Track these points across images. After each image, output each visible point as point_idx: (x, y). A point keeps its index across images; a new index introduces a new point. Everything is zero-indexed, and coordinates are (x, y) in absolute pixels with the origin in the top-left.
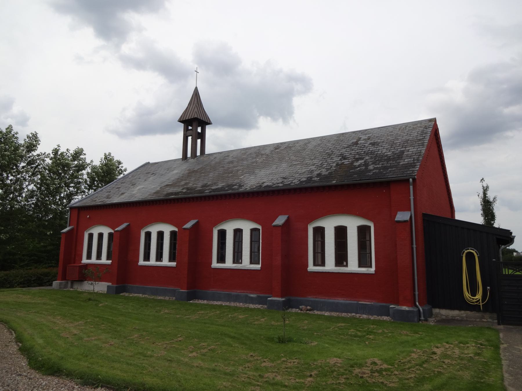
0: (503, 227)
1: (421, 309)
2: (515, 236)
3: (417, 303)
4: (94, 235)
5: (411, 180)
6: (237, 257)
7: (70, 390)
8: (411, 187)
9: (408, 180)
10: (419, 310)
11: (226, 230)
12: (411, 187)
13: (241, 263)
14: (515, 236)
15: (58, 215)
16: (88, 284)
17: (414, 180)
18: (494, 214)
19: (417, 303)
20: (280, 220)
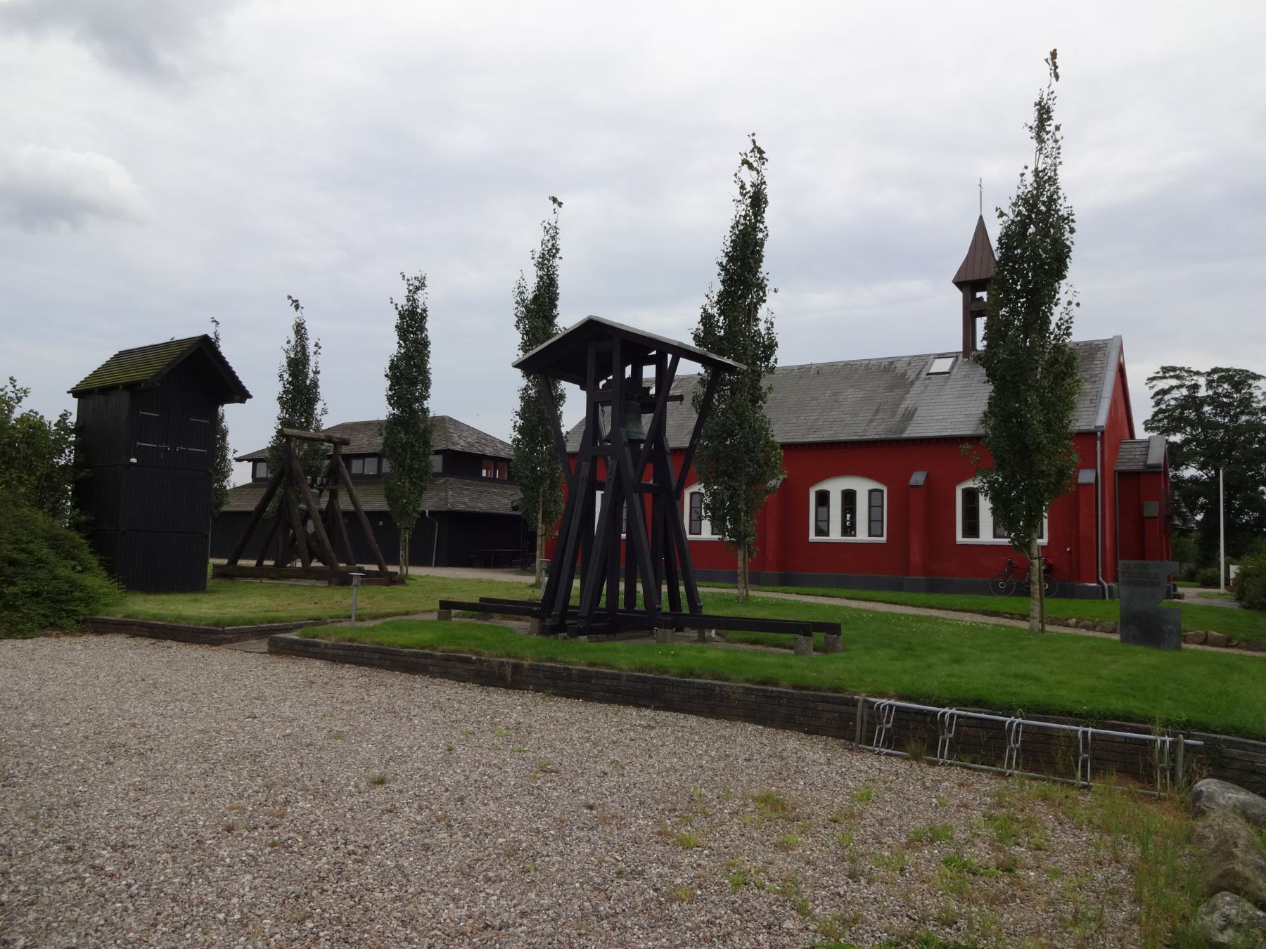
0: (438, 414)
1: (1106, 585)
2: (250, 397)
3: (1101, 579)
4: (226, 350)
5: (1099, 433)
6: (849, 529)
7: (725, 938)
8: (1099, 442)
9: (1096, 433)
10: (1103, 587)
11: (855, 491)
12: (1099, 442)
13: (855, 535)
14: (250, 397)
15: (1035, 264)
16: (327, 405)
17: (1102, 433)
18: (520, 422)
19: (1101, 579)
20: (918, 478)
